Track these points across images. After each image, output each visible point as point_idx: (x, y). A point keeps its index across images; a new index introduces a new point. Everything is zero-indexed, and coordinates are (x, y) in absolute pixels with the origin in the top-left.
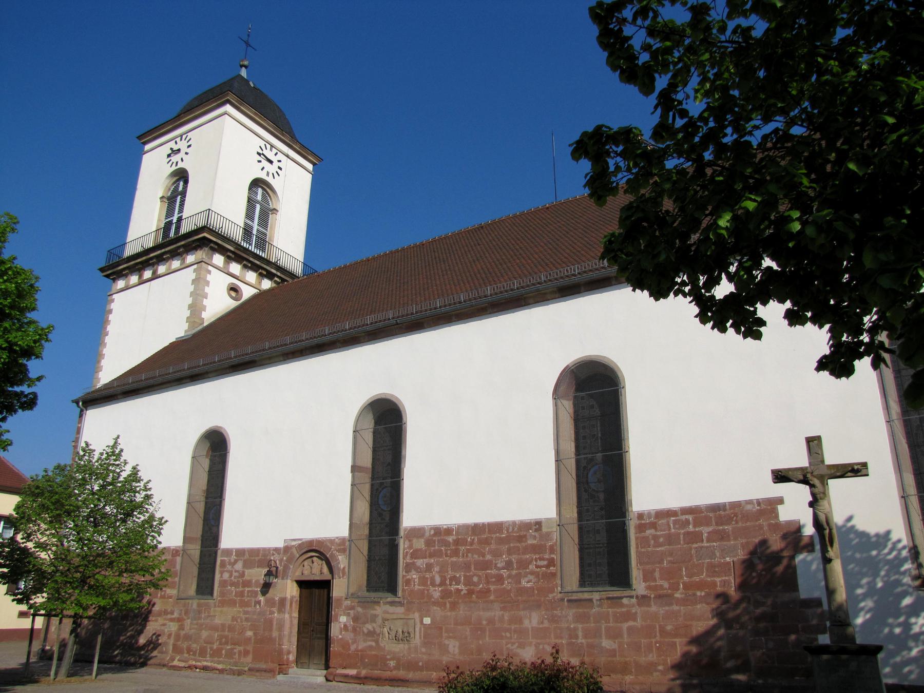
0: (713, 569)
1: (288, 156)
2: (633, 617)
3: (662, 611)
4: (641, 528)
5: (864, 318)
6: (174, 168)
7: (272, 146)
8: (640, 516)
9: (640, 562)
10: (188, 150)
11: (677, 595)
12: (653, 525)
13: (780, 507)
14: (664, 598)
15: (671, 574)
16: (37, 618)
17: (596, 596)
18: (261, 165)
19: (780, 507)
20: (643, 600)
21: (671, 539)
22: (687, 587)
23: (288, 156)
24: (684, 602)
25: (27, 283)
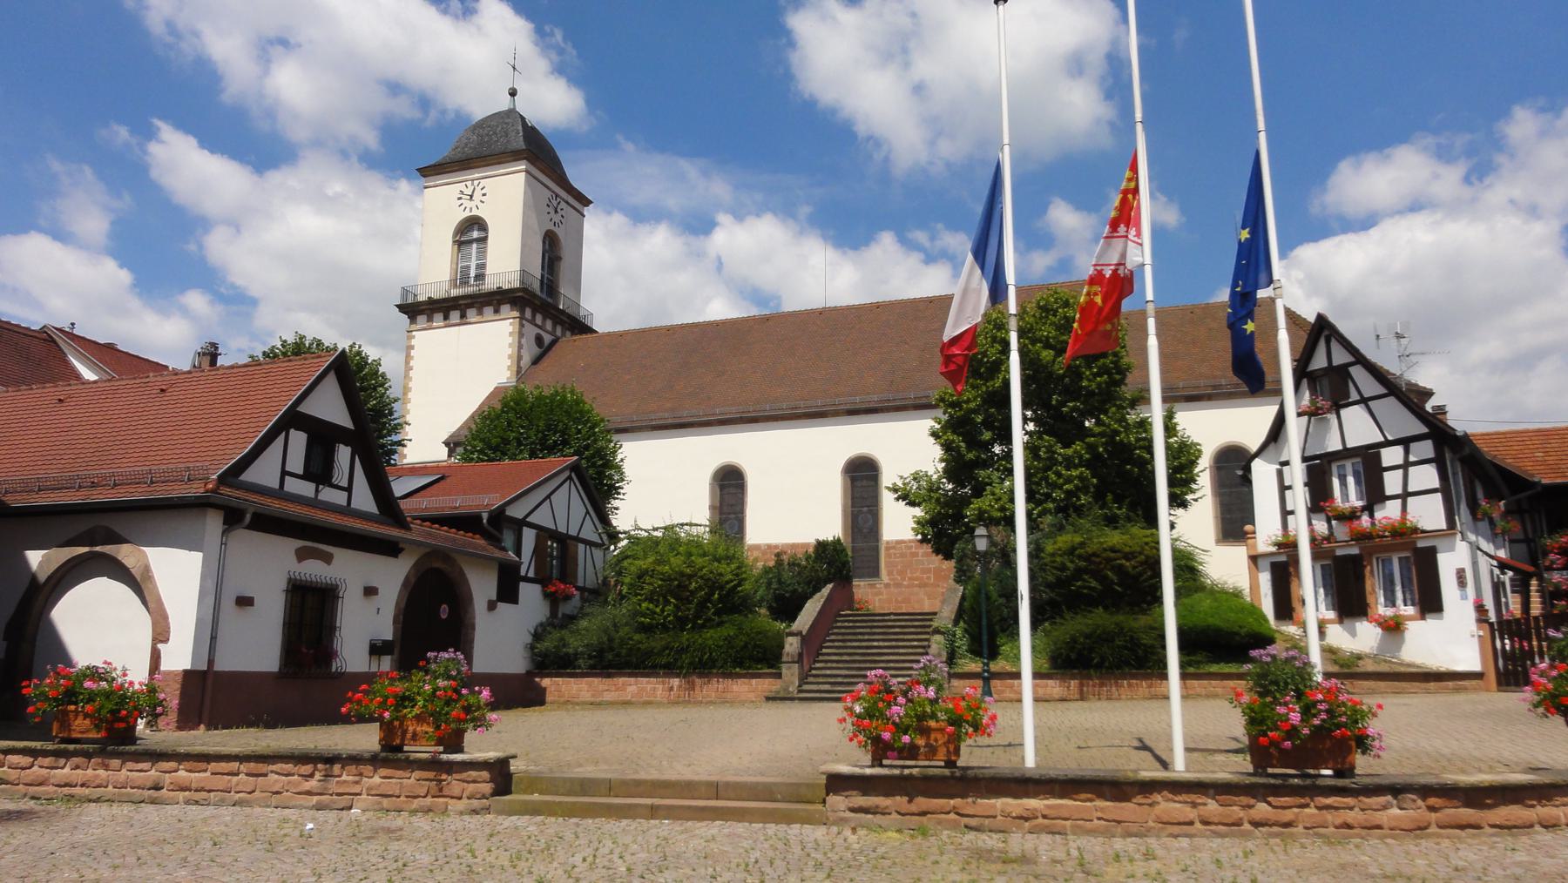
0: (924, 571)
1: (567, 203)
2: (881, 594)
3: (896, 591)
4: (888, 549)
5: (1248, 236)
6: (467, 214)
7: (557, 196)
8: (888, 542)
9: (886, 566)
10: (483, 199)
11: (905, 583)
12: (894, 548)
13: (387, 634)
14: (898, 585)
15: (901, 573)
16: (1399, 491)
17: (862, 583)
18: (548, 210)
19: (387, 634)
20: (887, 586)
21: (903, 555)
22: (910, 579)
23: (567, 203)
24: (908, 587)
25: (893, 580)
